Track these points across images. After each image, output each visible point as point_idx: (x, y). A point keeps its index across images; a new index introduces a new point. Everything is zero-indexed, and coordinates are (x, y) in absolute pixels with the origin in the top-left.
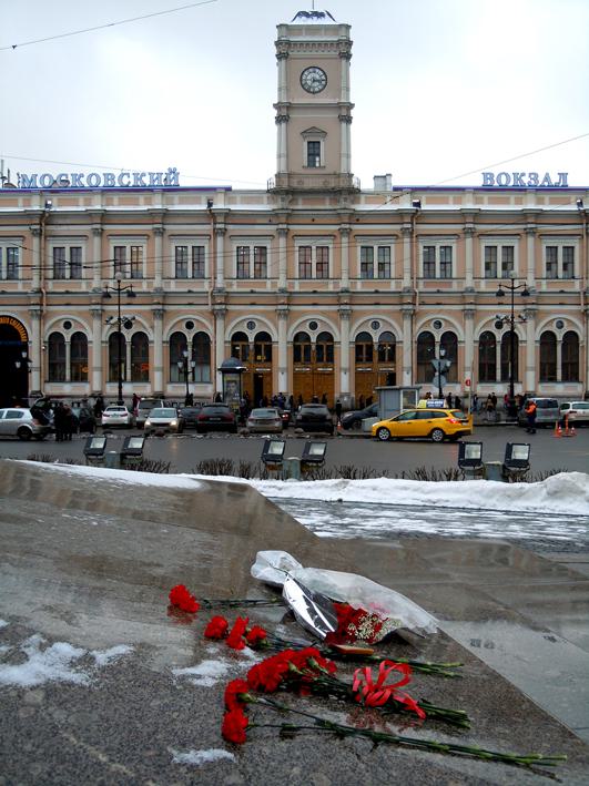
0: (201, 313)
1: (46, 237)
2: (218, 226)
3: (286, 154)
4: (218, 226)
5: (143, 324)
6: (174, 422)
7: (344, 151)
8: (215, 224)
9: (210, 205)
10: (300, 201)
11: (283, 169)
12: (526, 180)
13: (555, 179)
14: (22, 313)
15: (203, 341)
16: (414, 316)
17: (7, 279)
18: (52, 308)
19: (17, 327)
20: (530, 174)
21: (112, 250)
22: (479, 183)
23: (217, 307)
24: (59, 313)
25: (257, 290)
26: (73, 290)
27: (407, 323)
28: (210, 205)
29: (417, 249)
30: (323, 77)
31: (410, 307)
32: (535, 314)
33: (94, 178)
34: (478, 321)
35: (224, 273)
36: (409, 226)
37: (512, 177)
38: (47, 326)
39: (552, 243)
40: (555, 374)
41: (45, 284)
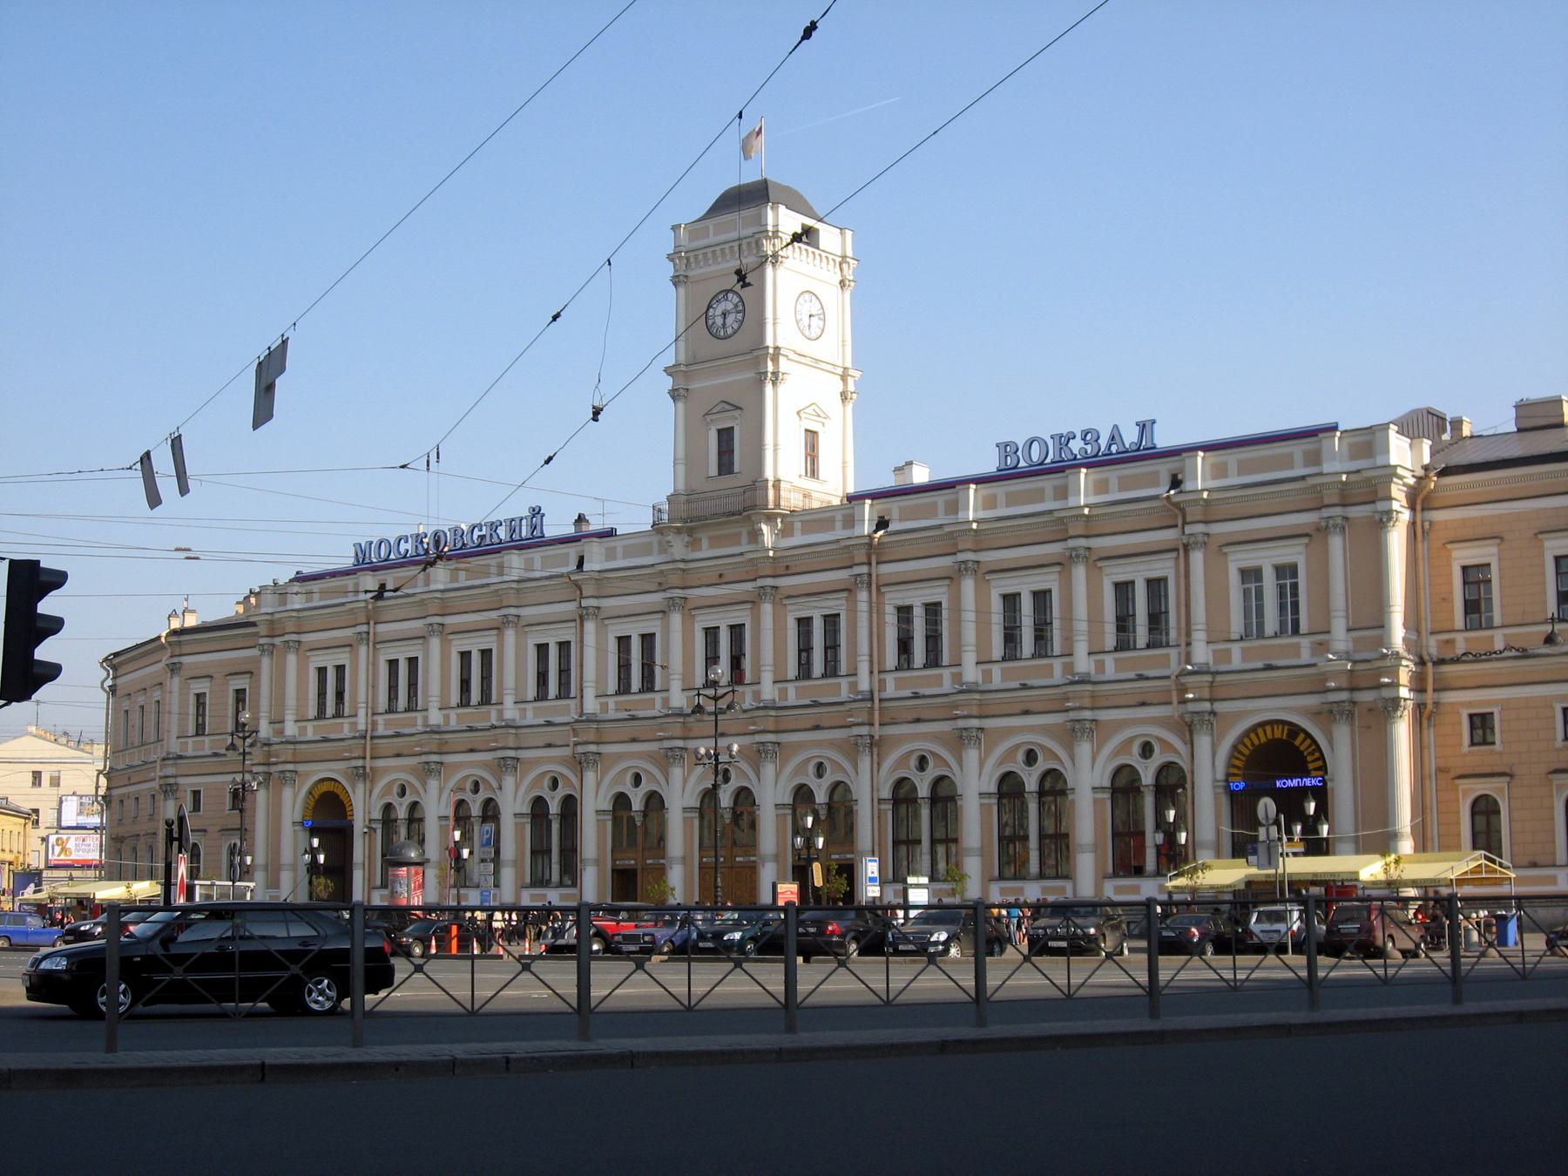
0: (937, 737)
1: (375, 643)
2: (585, 603)
3: (688, 459)
4: (585, 603)
5: (1054, 753)
6: (131, 928)
7: (681, 468)
8: (1185, 523)
9: (1176, 483)
10: (705, 543)
11: (681, 486)
12: (1076, 446)
13: (1130, 437)
14: (1316, 714)
15: (944, 798)
16: (876, 746)
17: (1148, 646)
18: (380, 763)
19: (325, 787)
20: (1085, 434)
21: (1234, 578)
22: (990, 465)
23: (580, 749)
24: (910, 739)
25: (640, 714)
26: (927, 692)
27: (865, 763)
28: (1176, 483)
29: (881, 613)
30: (730, 331)
31: (864, 730)
32: (1094, 730)
33: (1035, 446)
34: (988, 751)
35: (978, 652)
36: (864, 569)
37: (1050, 443)
38: (376, 791)
39: (1010, 584)
40: (1026, 862)
41: (882, 683)
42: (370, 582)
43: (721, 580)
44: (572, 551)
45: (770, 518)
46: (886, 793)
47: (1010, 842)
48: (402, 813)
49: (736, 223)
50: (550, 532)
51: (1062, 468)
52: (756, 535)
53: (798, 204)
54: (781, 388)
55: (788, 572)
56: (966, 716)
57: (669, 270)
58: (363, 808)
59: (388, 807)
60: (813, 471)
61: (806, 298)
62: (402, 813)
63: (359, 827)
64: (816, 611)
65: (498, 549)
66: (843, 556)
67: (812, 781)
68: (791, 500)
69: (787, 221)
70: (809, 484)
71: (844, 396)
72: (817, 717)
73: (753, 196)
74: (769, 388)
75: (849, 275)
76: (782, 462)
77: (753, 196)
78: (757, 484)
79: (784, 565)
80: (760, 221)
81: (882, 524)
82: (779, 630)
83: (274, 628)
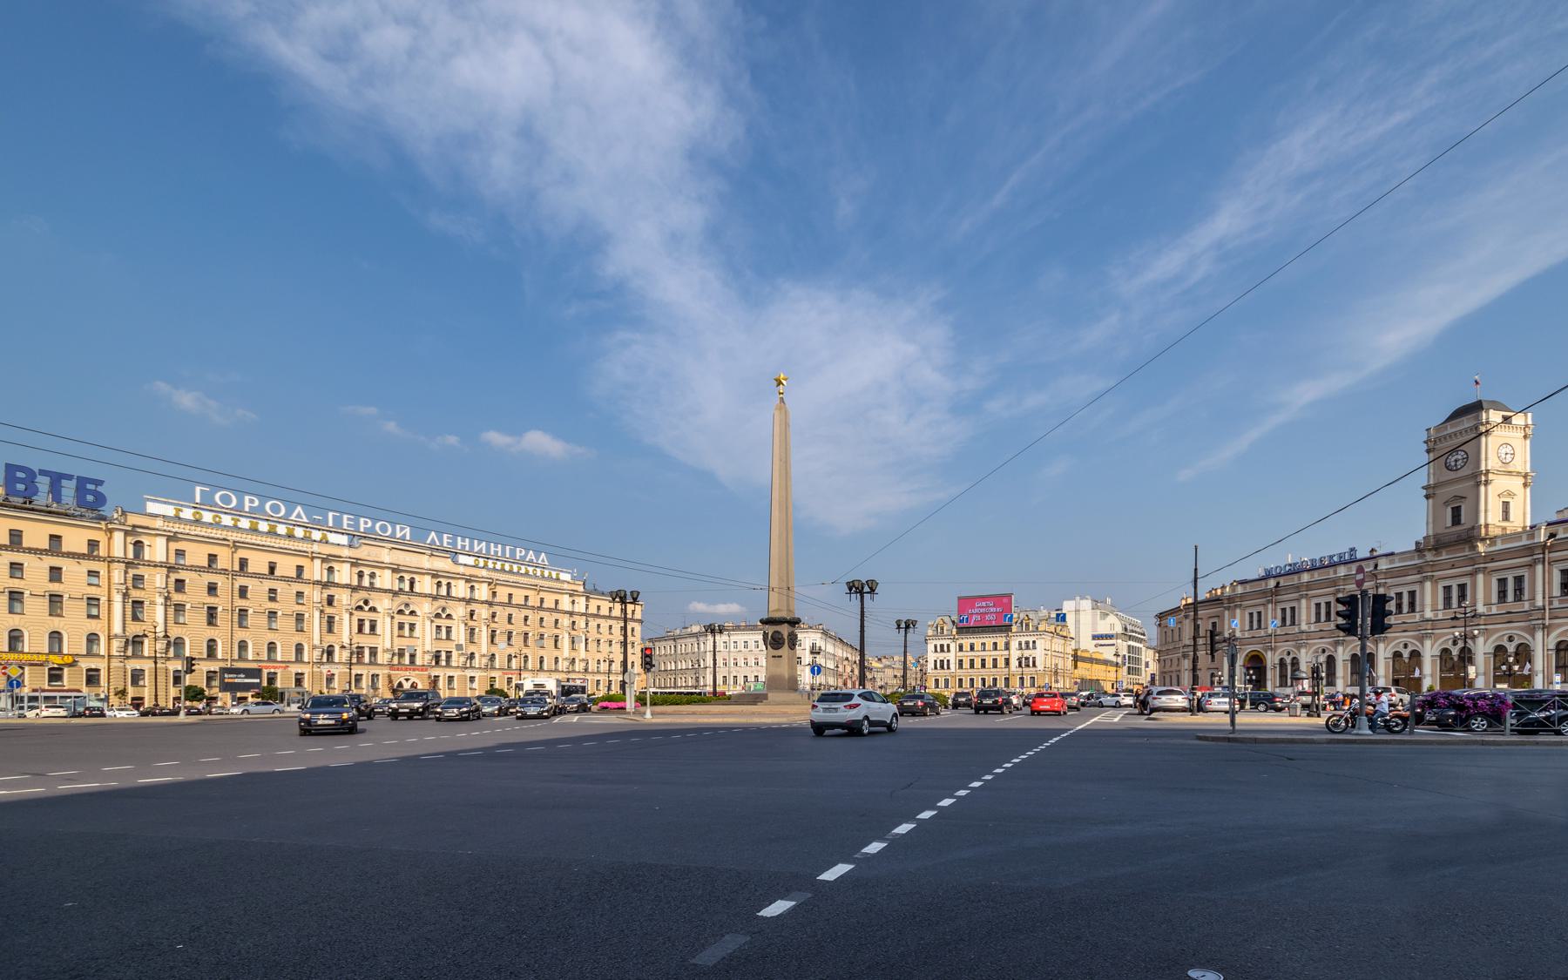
3: (1436, 518)
39: (1447, 583)
42: (1272, 583)
43: (1453, 567)
44: (1372, 563)
45: (1483, 540)
46: (1552, 646)
47: (1283, 676)
48: (1288, 660)
49: (1466, 422)
50: (1359, 555)
51: (1333, 565)
52: (1474, 548)
53: (1498, 406)
54: (1490, 487)
55: (1493, 560)
56: (1270, 641)
57: (1425, 447)
58: (1271, 659)
59: (1282, 660)
60: (1506, 517)
61: (1506, 448)
62: (1288, 660)
63: (1269, 666)
64: (1288, 606)
65: (1333, 565)
66: (1529, 550)
67: (1506, 644)
68: (1493, 532)
69: (1495, 416)
70: (1505, 524)
71: (1525, 485)
72: (1287, 637)
73: (1477, 407)
74: (1482, 488)
75: (1529, 432)
76: (1490, 516)
77: (1477, 407)
78: (1475, 527)
79: (1491, 558)
80: (1478, 418)
81: (1552, 536)
82: (1308, 608)
83: (1231, 599)
